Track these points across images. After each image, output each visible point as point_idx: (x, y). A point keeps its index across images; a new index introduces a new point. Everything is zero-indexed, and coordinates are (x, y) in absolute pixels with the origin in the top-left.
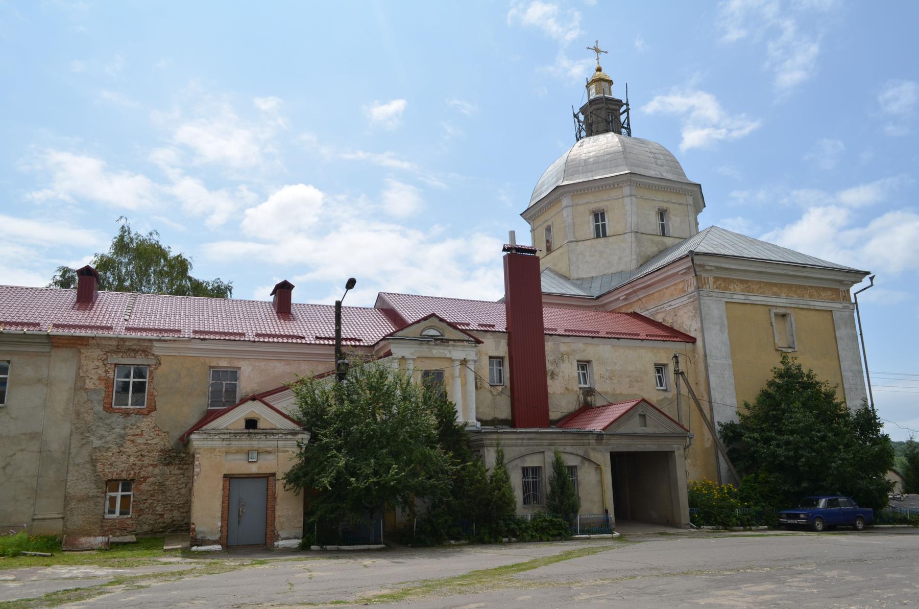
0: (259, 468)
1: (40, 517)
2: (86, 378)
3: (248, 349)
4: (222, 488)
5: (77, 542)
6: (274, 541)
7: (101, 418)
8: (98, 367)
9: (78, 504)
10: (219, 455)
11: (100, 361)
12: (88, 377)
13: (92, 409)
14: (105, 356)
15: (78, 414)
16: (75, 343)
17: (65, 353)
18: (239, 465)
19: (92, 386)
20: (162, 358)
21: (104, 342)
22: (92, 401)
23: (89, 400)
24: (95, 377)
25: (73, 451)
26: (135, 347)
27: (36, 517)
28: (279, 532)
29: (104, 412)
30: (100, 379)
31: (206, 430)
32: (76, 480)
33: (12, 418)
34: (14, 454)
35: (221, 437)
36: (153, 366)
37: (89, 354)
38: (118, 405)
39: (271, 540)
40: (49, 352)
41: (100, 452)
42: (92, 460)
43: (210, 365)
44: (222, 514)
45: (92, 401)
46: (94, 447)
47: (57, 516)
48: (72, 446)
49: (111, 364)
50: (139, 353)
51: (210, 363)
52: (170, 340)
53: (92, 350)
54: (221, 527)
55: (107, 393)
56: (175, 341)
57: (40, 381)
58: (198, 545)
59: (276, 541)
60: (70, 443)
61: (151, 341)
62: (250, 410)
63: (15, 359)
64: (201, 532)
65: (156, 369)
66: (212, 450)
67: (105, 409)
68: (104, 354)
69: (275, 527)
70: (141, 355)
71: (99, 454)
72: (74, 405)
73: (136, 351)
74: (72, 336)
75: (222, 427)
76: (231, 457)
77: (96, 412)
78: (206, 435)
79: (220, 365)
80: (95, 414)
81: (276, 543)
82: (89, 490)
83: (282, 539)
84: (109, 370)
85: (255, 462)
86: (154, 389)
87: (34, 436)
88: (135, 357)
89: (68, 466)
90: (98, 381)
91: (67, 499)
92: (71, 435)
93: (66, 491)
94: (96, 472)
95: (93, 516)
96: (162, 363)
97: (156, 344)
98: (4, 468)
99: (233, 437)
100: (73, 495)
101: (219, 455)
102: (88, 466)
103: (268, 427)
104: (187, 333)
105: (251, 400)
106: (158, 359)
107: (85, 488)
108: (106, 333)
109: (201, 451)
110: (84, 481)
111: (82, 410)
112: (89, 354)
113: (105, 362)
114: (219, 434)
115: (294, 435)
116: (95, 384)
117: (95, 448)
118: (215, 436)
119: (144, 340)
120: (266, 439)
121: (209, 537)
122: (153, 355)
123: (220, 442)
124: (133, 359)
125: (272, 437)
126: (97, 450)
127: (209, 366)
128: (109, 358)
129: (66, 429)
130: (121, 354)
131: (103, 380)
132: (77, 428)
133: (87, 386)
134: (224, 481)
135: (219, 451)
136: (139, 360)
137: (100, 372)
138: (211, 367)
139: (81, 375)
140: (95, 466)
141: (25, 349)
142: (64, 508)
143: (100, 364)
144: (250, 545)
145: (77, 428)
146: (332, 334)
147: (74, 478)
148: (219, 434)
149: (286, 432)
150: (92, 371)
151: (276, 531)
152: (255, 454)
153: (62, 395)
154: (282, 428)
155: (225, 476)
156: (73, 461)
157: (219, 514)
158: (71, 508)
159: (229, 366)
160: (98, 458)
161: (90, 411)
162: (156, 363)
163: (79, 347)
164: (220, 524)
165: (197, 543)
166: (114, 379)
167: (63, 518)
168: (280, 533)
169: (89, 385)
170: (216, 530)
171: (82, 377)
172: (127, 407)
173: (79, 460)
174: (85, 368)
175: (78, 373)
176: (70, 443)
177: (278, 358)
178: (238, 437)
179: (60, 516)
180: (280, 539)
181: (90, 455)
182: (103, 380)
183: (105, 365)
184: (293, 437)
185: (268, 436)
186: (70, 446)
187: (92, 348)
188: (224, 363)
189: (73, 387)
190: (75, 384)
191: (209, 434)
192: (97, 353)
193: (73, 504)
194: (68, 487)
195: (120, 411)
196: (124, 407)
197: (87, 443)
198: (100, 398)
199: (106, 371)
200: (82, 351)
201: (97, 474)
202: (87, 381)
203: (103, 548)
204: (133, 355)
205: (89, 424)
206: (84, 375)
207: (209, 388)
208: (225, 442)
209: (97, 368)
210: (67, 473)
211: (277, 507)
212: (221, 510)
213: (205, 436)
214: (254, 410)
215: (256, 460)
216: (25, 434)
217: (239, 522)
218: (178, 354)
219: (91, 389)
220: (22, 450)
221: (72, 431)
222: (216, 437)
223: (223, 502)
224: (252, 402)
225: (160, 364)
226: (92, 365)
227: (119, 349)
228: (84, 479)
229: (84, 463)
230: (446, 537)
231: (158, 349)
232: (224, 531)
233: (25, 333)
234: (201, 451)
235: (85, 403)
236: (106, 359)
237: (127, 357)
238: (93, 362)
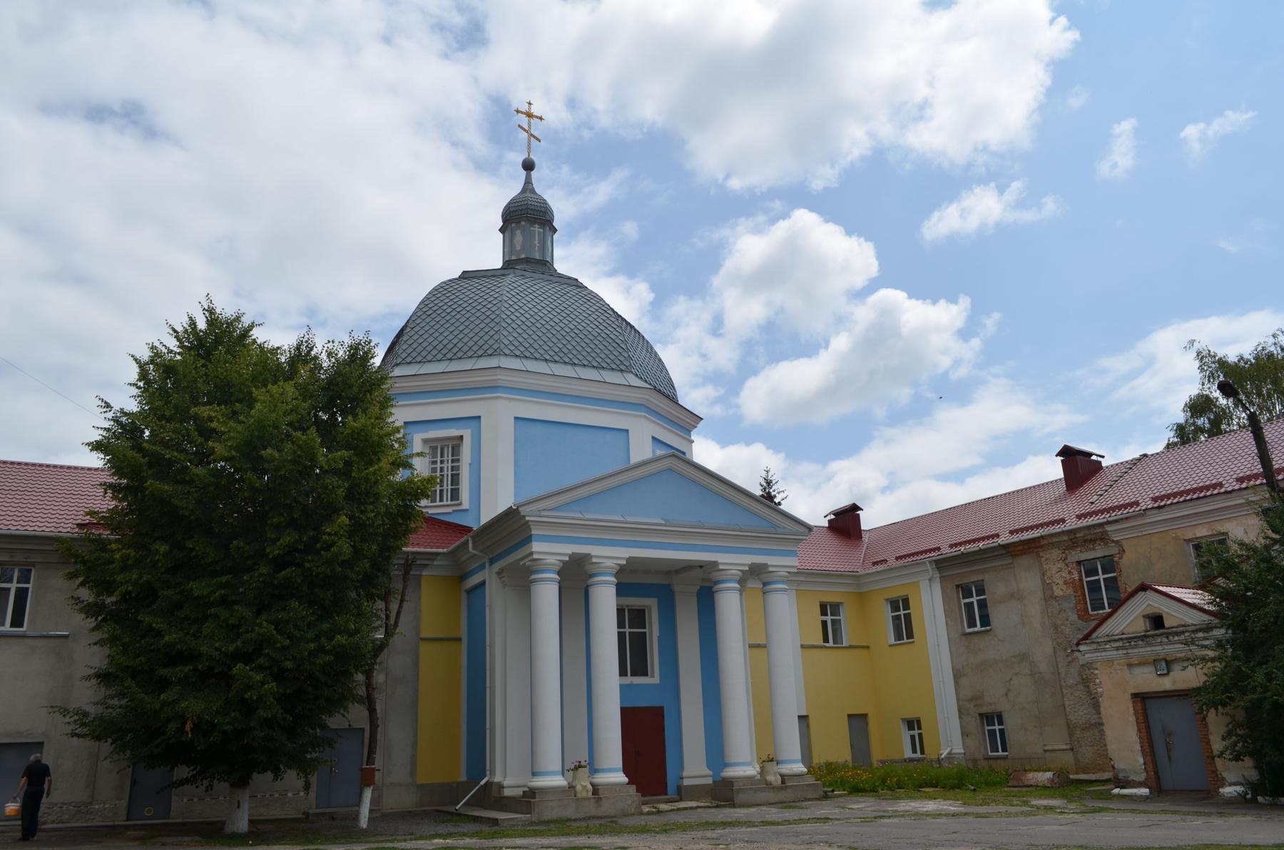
0: (1174, 682)
1: (1050, 748)
2: (1053, 584)
3: (1226, 504)
4: (1133, 712)
5: (1024, 778)
6: (1219, 787)
7: (1079, 629)
8: (1060, 570)
9: (1083, 733)
10: (1120, 669)
11: (1061, 561)
12: (1054, 582)
13: (1068, 620)
14: (1064, 555)
15: (1056, 627)
16: (1030, 548)
17: (1025, 561)
18: (1148, 680)
19: (1061, 593)
20: (1125, 544)
21: (1055, 540)
22: (1065, 610)
23: (1062, 610)
24: (1061, 582)
25: (1062, 671)
26: (1089, 537)
27: (1046, 748)
28: (1222, 773)
29: (1080, 622)
30: (1066, 583)
31: (1097, 637)
32: (1074, 704)
33: (999, 640)
34: (1011, 679)
35: (1113, 646)
36: (1117, 556)
37: (1048, 556)
38: (1104, 606)
39: (1214, 784)
40: (1012, 563)
41: (1089, 669)
42: (1084, 679)
43: (1186, 538)
44: (1141, 747)
45: (1065, 610)
46: (1081, 663)
47: (1064, 747)
48: (1060, 666)
49: (1073, 563)
50: (1097, 542)
51: (1184, 535)
52: (1122, 519)
53: (1049, 551)
54: (1145, 764)
55: (1077, 598)
56: (1127, 518)
57: (1012, 596)
58: (1122, 787)
59: (1222, 787)
60: (1056, 662)
61: (1101, 525)
62: (1146, 604)
63: (987, 578)
64: (1123, 771)
65: (1121, 558)
66: (1110, 661)
67: (1080, 617)
68: (1063, 553)
69: (1215, 766)
70: (1100, 544)
71: (1088, 672)
72: (1048, 617)
73: (1093, 541)
74: (1021, 541)
75: (1116, 633)
76: (1137, 671)
77: (1073, 623)
78: (1095, 645)
79: (1198, 536)
80: (1071, 624)
81: (1221, 790)
82: (1089, 716)
83: (1230, 785)
84: (1072, 571)
85: (1165, 674)
86: (1126, 584)
87: (1023, 657)
88: (1094, 549)
89: (1061, 689)
90: (1065, 586)
91: (1070, 728)
92: (1055, 652)
93: (1067, 719)
94: (1091, 694)
95: (1101, 747)
96: (1126, 550)
97: (1109, 528)
98: (1007, 695)
99: (1127, 644)
100: (1075, 723)
101: (1120, 669)
102: (1081, 687)
103: (1175, 625)
104: (1147, 503)
105: (1141, 590)
106: (1120, 545)
107: (1085, 714)
108: (1057, 528)
109: (1098, 665)
110: (1082, 705)
111: (1059, 622)
112: (1048, 556)
113: (1067, 562)
114: (1109, 641)
115: (1207, 632)
116: (1062, 590)
117: (1083, 665)
118: (1106, 645)
119: (1094, 526)
120: (1169, 641)
121: (1133, 777)
122: (1113, 541)
123: (1115, 653)
124: (1093, 552)
125: (1176, 638)
126: (1085, 668)
127: (1185, 540)
128: (1068, 557)
129: (1048, 646)
130: (1079, 549)
131: (1069, 583)
132: (1059, 644)
133: (1056, 594)
134: (1133, 702)
135: (1119, 664)
136: (1100, 552)
137: (1064, 575)
138: (1188, 541)
139: (1048, 582)
140: (1088, 687)
141: (992, 565)
142: (1070, 738)
143: (1061, 565)
144: (1192, 791)
145: (1059, 644)
146: (1258, 468)
147: (1072, 702)
148: (1109, 641)
149: (1193, 628)
150: (1057, 575)
151: (1218, 773)
152: (1164, 664)
153: (1034, 607)
154: (1195, 623)
155: (1135, 696)
156: (1065, 682)
157: (1138, 747)
158: (1078, 738)
159: (1210, 534)
160: (1089, 677)
161: (1066, 622)
162: (1120, 550)
163: (1036, 550)
164: (1141, 760)
165: (1121, 784)
166: (1081, 580)
167: (1072, 749)
168: (1225, 775)
169: (1058, 592)
170: (1139, 768)
171: (1049, 584)
172: (1105, 611)
173: (1071, 681)
174: (1048, 573)
175: (1043, 581)
176: (1056, 662)
177: (1213, 519)
178: (1133, 643)
179: (1068, 747)
180: (1227, 784)
181: (1080, 674)
182: (1069, 583)
183: (1067, 565)
184: (1206, 635)
185: (1171, 637)
186: (1057, 665)
187: (1048, 549)
188: (1202, 532)
189: (1042, 596)
190: (1044, 593)
191: (1098, 643)
192: (1055, 553)
193: (1078, 733)
194: (1068, 714)
195: (1096, 617)
196: (1101, 612)
197: (1074, 660)
198: (1072, 605)
199: (1070, 573)
200: (1041, 554)
201: (1093, 696)
202: (1055, 588)
203: (1049, 785)
204: (1092, 546)
205: (1069, 638)
206: (1050, 581)
207: (1194, 570)
208: (1120, 652)
209: (1059, 571)
210: (1063, 697)
211: (1212, 738)
212: (1139, 742)
213: (1094, 646)
214: (1150, 603)
215: (1165, 672)
216: (1014, 657)
217: (1169, 758)
218: (1140, 534)
219: (1061, 596)
220: (1016, 674)
221: (1054, 648)
222: (1107, 646)
223: (1139, 730)
224: (1144, 593)
225: (1124, 551)
226: (1054, 569)
227: (1074, 543)
228: (1081, 703)
229: (1077, 684)
230: (1269, 793)
231: (1115, 533)
232: (1149, 769)
233: (980, 549)
234: (1098, 665)
235: (1059, 614)
236: (1066, 559)
237: (1086, 551)
238: (1055, 564)
